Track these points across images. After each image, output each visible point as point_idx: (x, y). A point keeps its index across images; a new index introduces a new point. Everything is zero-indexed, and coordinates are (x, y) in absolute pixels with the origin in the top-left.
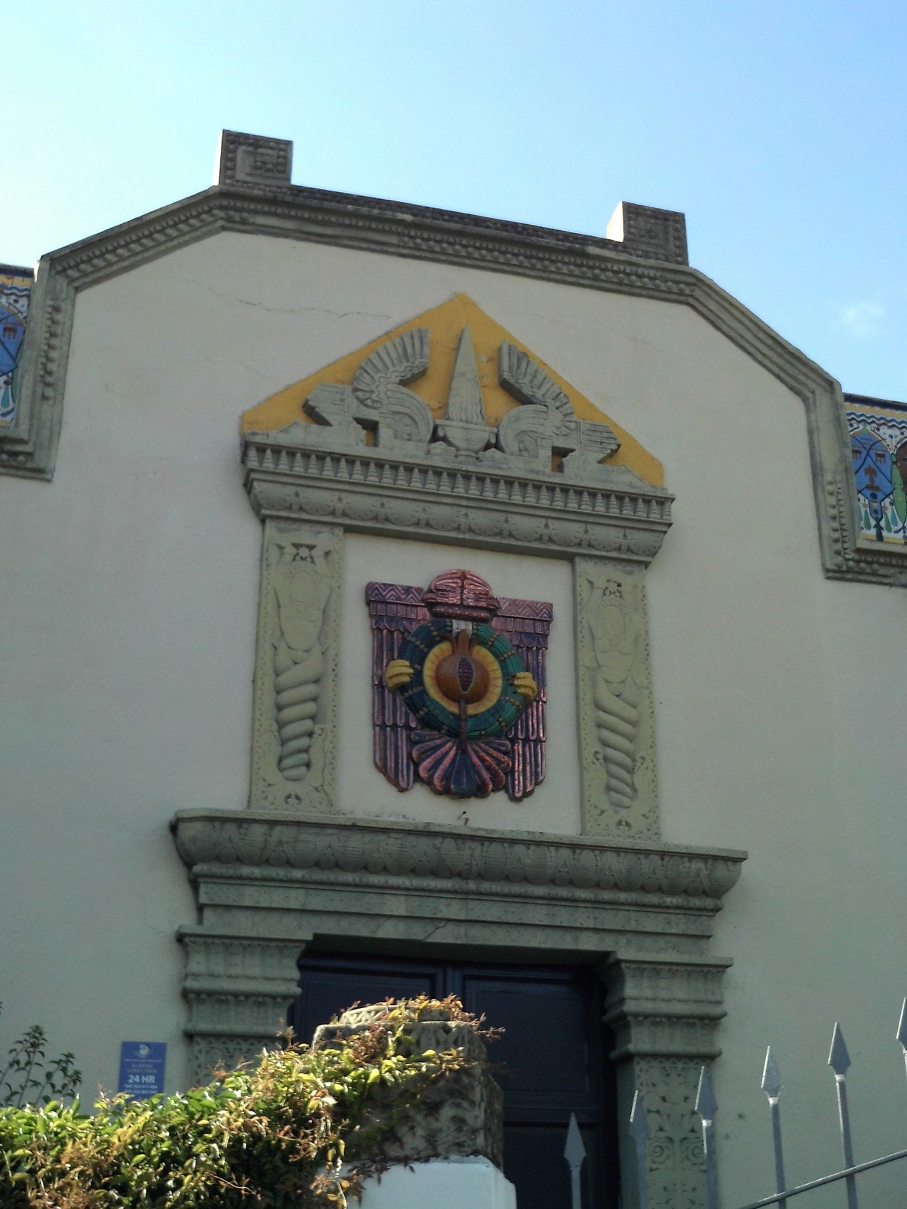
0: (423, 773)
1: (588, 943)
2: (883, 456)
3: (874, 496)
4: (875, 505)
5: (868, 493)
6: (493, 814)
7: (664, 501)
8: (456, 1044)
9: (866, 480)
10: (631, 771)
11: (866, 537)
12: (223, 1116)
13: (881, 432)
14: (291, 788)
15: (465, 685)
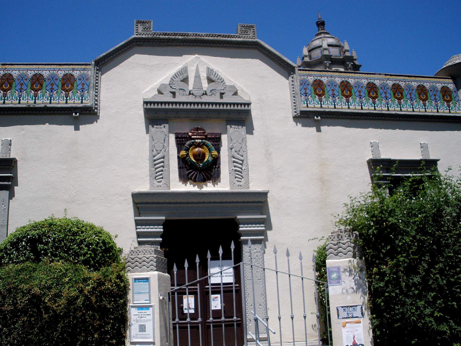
3: (387, 99)
5: (304, 95)
6: (209, 188)
7: (249, 104)
10: (241, 172)
11: (303, 107)
12: (79, 239)
15: (200, 157)
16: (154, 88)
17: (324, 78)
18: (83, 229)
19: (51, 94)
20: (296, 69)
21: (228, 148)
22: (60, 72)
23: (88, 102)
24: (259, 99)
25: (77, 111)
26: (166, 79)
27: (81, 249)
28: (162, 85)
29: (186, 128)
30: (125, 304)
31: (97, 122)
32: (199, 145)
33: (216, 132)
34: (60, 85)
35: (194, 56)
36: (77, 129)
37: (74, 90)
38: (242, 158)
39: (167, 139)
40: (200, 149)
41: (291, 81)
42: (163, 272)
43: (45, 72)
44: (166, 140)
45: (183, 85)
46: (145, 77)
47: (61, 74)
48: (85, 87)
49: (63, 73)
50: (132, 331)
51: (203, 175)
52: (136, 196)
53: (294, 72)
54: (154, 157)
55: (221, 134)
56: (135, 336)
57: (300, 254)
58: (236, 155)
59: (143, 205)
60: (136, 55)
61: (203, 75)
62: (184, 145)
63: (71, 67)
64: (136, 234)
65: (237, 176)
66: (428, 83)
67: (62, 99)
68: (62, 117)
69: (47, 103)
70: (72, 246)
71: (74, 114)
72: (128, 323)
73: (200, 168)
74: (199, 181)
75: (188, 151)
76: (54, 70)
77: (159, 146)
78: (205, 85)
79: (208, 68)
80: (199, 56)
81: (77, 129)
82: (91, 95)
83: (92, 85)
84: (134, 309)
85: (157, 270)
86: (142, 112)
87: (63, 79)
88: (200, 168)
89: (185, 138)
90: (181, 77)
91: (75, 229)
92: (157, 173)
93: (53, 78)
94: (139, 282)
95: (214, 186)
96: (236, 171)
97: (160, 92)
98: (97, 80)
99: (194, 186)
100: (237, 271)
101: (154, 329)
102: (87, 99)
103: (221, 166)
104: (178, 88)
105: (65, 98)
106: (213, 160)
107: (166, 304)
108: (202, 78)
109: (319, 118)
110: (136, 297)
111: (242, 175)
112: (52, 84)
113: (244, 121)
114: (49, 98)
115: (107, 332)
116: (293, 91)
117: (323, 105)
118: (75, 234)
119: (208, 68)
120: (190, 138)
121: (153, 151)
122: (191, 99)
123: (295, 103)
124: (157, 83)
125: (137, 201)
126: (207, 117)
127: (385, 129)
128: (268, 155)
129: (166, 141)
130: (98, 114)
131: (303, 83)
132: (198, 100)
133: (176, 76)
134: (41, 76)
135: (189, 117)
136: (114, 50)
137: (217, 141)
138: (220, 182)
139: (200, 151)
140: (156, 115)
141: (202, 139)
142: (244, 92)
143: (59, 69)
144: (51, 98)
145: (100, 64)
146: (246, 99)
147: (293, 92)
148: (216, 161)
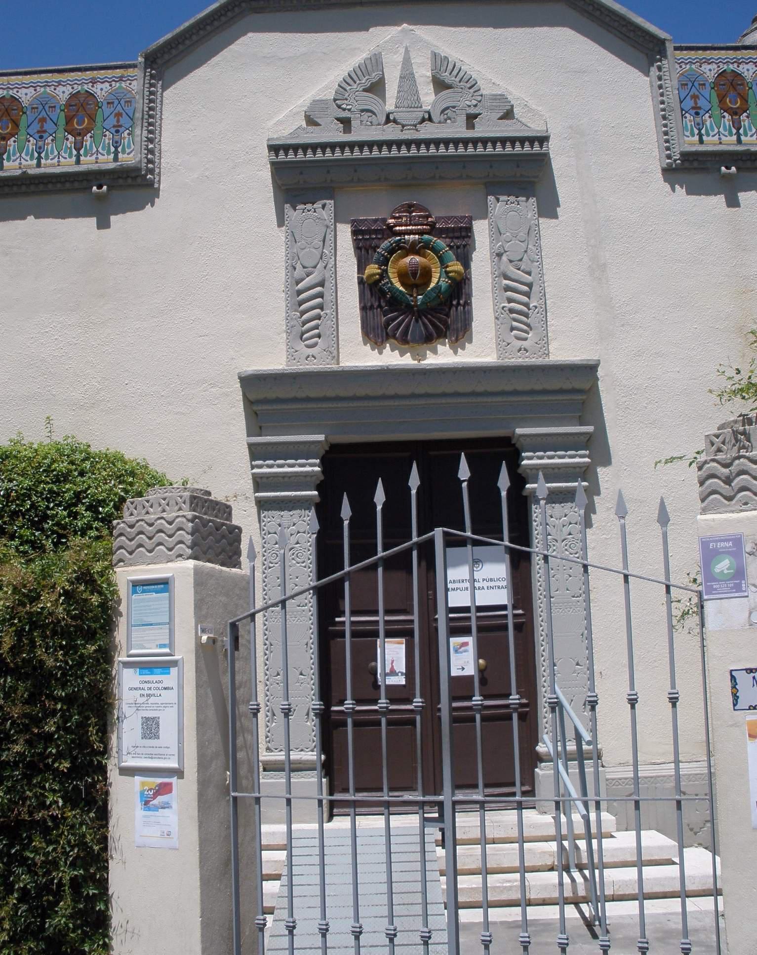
0: (390, 333)
2: (704, 85)
6: (442, 356)
7: (543, 140)
9: (692, 104)
11: (690, 143)
12: (69, 490)
14: (310, 351)
15: (417, 279)
16: (298, 113)
17: (746, 67)
18: (87, 465)
19: (41, 143)
20: (670, 47)
21: (491, 254)
22: (61, 89)
23: (130, 158)
24: (571, 127)
25: (102, 182)
26: (327, 87)
27: (74, 515)
28: (315, 103)
29: (379, 208)
30: (106, 655)
31: (152, 205)
32: (413, 249)
33: (459, 214)
34: (62, 121)
35: (400, 28)
36: (104, 224)
37: (97, 131)
38: (528, 279)
39: (330, 236)
40: (418, 259)
41: (655, 79)
42: (222, 565)
43: (24, 91)
44: (328, 240)
45: (370, 101)
46: (275, 85)
47: (63, 94)
48: (124, 120)
49: (68, 90)
50: (125, 737)
51: (424, 324)
52: (251, 383)
53: (663, 53)
54: (297, 283)
55: (471, 219)
56: (131, 749)
57: (662, 505)
58: (512, 271)
59: (265, 407)
60: (250, 35)
61: (423, 73)
62: (375, 251)
63: (89, 74)
64: (251, 482)
65: (515, 324)
67: (66, 156)
68: (66, 199)
69: (30, 167)
70: (52, 509)
71: (95, 188)
72: (116, 712)
73: (416, 303)
74: (414, 341)
75: (387, 265)
76: (47, 85)
77: (310, 256)
78: (428, 97)
79: (435, 55)
80: (411, 27)
81: (104, 224)
82: (138, 139)
83: (138, 115)
84: (131, 670)
85: (196, 558)
86: (266, 174)
87: (68, 105)
88: (416, 303)
89: (376, 232)
90: (365, 82)
91: (63, 466)
92: (304, 323)
93: (44, 103)
94: (144, 591)
95: (456, 353)
96: (512, 311)
97: (311, 121)
98: (151, 101)
99: (402, 354)
100: (520, 564)
101: (181, 731)
102: (128, 151)
103: (473, 300)
104: (356, 107)
105: (74, 152)
106: (450, 286)
107: (226, 655)
108: (419, 80)
109: (733, 169)
110: (135, 636)
111: (529, 321)
112: (43, 121)
113: (532, 184)
114: (36, 155)
115: (48, 738)
116: (662, 102)
117: (743, 138)
118: (62, 478)
119: (435, 55)
120: (390, 231)
121: (295, 269)
122: (392, 133)
123: (666, 133)
124: (302, 101)
125: (252, 397)
126: (433, 178)
128: (598, 270)
129: (328, 242)
130: (156, 186)
131: (689, 83)
132: (408, 135)
133: (351, 78)
134: (16, 103)
135: (386, 179)
136: (192, 27)
137: (461, 240)
138: (470, 341)
139: (417, 264)
140: (302, 177)
141: (421, 233)
142: (531, 110)
143: (59, 83)
144: (39, 153)
145: (159, 61)
146: (535, 127)
147: (662, 106)
148: (459, 288)
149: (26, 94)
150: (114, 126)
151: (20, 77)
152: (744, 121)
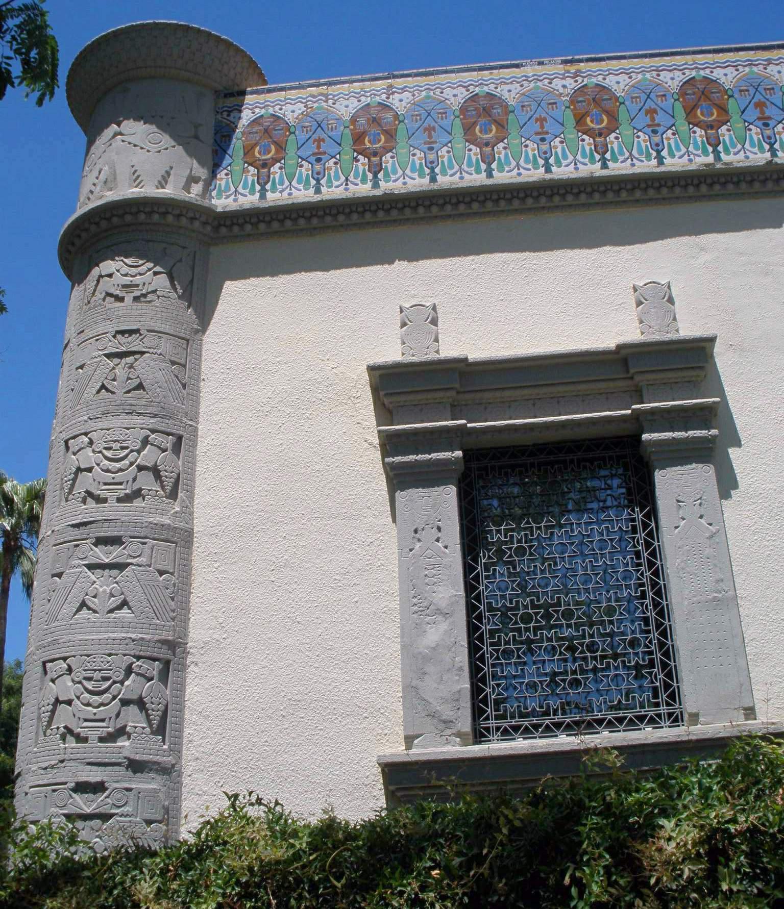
1: (116, 534)
4: (768, 132)
5: (760, 123)
8: (621, 796)
13: (607, 81)
34: (570, 121)
66: (730, 70)
76: (751, 64)
112: (652, 112)
127: (306, 271)
149: (401, 100)
150: (314, 154)
151: (710, 56)
152: (612, 143)
